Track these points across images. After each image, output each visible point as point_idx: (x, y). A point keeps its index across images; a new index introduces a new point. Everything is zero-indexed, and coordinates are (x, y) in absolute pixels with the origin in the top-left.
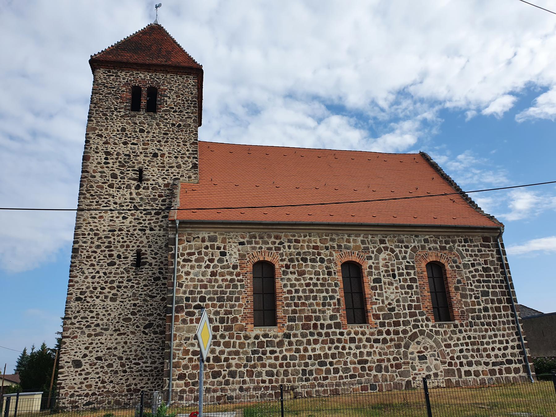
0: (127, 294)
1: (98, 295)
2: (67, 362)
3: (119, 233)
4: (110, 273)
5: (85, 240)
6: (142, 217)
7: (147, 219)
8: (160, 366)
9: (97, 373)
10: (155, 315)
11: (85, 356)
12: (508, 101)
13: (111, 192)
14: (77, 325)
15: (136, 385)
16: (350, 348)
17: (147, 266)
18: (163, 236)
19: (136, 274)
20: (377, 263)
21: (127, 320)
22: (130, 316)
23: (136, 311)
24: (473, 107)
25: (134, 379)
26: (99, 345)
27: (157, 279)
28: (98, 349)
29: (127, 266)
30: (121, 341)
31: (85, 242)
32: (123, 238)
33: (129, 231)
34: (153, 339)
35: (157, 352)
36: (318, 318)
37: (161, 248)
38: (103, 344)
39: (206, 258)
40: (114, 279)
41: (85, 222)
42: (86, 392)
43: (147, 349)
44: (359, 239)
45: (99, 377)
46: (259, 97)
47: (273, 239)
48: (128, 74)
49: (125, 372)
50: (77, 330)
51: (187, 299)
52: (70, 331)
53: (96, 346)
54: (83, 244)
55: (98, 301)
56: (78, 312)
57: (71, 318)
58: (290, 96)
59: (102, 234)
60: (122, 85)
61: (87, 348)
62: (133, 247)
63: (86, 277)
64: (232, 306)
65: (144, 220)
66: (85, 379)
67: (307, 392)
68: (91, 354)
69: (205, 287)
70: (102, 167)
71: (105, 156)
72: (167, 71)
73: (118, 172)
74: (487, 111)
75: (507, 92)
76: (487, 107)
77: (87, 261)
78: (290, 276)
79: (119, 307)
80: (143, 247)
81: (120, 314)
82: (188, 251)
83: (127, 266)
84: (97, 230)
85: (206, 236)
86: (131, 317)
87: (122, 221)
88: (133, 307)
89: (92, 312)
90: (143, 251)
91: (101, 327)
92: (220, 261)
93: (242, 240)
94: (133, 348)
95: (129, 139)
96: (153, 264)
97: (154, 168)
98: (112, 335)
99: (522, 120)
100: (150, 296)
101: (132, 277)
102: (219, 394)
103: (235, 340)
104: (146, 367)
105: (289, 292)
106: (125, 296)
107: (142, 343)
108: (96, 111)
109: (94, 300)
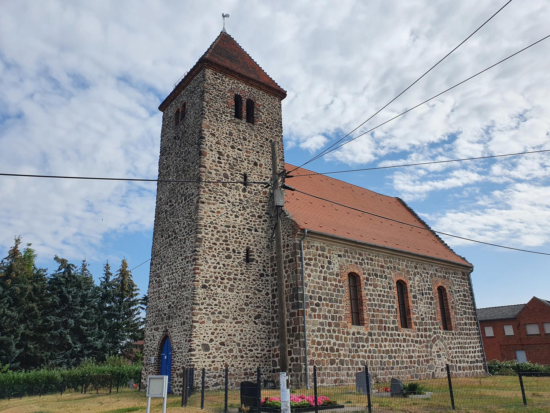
0: (241, 286)
1: (219, 284)
2: (198, 345)
3: (233, 229)
4: (228, 265)
5: (207, 231)
6: (249, 218)
7: (253, 220)
8: (267, 353)
9: (222, 357)
10: (262, 307)
11: (212, 340)
12: (321, 140)
13: (225, 191)
14: (204, 311)
15: (251, 369)
16: (404, 347)
17: (254, 263)
18: (265, 238)
19: (247, 269)
20: (414, 284)
21: (242, 310)
22: (244, 306)
23: (248, 302)
24: (294, 138)
25: (249, 364)
26: (222, 331)
27: (262, 275)
28: (221, 335)
29: (240, 260)
30: (238, 329)
31: (207, 234)
32: (236, 235)
33: (240, 229)
34: (261, 329)
35: (265, 340)
36: (386, 323)
37: (264, 248)
38: (225, 330)
39: (320, 265)
40: (231, 271)
41: (206, 215)
42: (214, 374)
43: (258, 338)
44: (405, 263)
45: (223, 361)
46: (88, 70)
47: (358, 256)
48: (231, 82)
49: (242, 357)
50: (204, 315)
51: (311, 297)
52: (199, 316)
53: (219, 332)
54: (206, 235)
55: (219, 290)
56: (205, 299)
57: (199, 304)
58: (124, 79)
59: (220, 229)
60: (227, 90)
61: (213, 333)
62: (244, 244)
63: (209, 267)
64: (338, 307)
65: (251, 221)
66: (213, 362)
67: (384, 378)
68: (217, 339)
69: (320, 288)
70: (216, 166)
71: (218, 156)
72: (260, 88)
73: (229, 173)
74: (303, 146)
75: (322, 132)
76: (305, 141)
77: (210, 252)
78: (369, 287)
79: (236, 297)
80: (251, 245)
81: (237, 304)
82: (308, 256)
83: (240, 260)
84: (216, 224)
85: (319, 245)
86: (245, 307)
87: (235, 219)
88: (246, 299)
89: (215, 300)
90: (251, 249)
91: (223, 314)
92: (328, 268)
93: (340, 253)
94: (248, 336)
95: (236, 144)
96: (259, 262)
97: (255, 176)
98: (231, 323)
99: (329, 160)
100: (258, 290)
101: (244, 271)
102: (335, 378)
103: (341, 334)
104: (258, 353)
105: (370, 300)
106: (240, 288)
107: (254, 332)
108: (208, 109)
109: (216, 289)
